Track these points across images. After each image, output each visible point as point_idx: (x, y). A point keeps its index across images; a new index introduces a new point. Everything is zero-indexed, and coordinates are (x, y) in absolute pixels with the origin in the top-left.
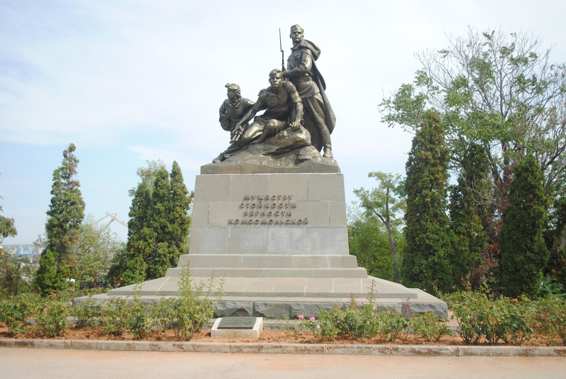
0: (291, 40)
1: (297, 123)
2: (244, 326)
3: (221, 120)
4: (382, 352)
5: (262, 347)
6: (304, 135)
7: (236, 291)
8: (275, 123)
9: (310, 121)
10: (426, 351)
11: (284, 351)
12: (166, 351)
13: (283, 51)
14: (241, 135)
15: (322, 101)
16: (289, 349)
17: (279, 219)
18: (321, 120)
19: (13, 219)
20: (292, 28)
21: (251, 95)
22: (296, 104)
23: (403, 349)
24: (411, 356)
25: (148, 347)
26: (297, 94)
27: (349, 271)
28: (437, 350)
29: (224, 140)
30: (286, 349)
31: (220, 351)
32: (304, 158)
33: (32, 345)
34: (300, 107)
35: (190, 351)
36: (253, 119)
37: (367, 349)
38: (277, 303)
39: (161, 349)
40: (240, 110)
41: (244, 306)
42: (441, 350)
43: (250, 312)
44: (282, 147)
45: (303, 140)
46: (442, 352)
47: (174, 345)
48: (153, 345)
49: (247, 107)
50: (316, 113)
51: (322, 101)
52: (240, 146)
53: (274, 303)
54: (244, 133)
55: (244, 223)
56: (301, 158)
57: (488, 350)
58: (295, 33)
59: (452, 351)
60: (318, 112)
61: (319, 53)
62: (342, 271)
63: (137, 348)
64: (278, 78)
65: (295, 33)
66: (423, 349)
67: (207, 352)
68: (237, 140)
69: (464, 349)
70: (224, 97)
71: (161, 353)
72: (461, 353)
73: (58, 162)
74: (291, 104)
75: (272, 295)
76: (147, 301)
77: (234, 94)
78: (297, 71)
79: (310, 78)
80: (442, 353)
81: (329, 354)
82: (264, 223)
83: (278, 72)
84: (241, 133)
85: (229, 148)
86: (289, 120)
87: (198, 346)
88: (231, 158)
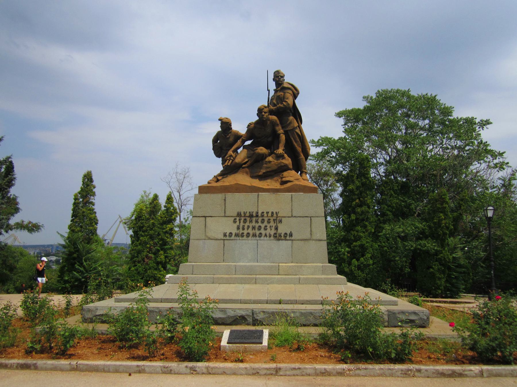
0: (274, 83)
1: (280, 151)
2: (254, 341)
3: (214, 149)
4: (406, 374)
5: (280, 369)
6: (288, 161)
7: (234, 298)
8: (262, 150)
9: (290, 149)
10: (450, 372)
11: (304, 373)
12: (178, 374)
13: (269, 91)
14: (233, 161)
15: (300, 134)
16: (309, 371)
17: (268, 231)
18: (299, 149)
19: (43, 226)
20: (274, 73)
21: (240, 127)
22: (279, 134)
23: (426, 370)
24: (435, 377)
25: (159, 369)
26: (280, 127)
27: (331, 278)
28: (461, 371)
29: (216, 166)
30: (305, 371)
31: (234, 374)
32: (287, 179)
33: (36, 367)
34: (283, 137)
35: (203, 373)
36: (242, 148)
37: (390, 371)
38: (274, 310)
39: (173, 372)
40: (231, 139)
41: (243, 313)
42: (464, 371)
43: (250, 320)
44: (268, 170)
45: (286, 165)
46: (466, 373)
47: (186, 367)
48: (164, 367)
49: (237, 137)
50: (295, 143)
51: (300, 134)
52: (229, 170)
53: (272, 310)
54: (234, 159)
55: (237, 235)
56: (284, 179)
57: (512, 371)
58: (278, 78)
59: (477, 371)
60: (296, 141)
61: (298, 93)
62: (325, 278)
63: (147, 369)
64: (265, 113)
65: (278, 78)
66: (447, 370)
67: (222, 374)
68: (229, 164)
69: (488, 370)
70: (217, 128)
71: (173, 375)
72: (485, 375)
73: (78, 186)
74: (277, 136)
75: (267, 302)
76: (152, 309)
77: (226, 125)
78: (280, 107)
79: (291, 114)
80: (466, 375)
81: (350, 376)
82: (254, 235)
83: (265, 107)
84: (232, 158)
85: (222, 171)
86: (272, 147)
87: (212, 368)
88: (225, 179)
